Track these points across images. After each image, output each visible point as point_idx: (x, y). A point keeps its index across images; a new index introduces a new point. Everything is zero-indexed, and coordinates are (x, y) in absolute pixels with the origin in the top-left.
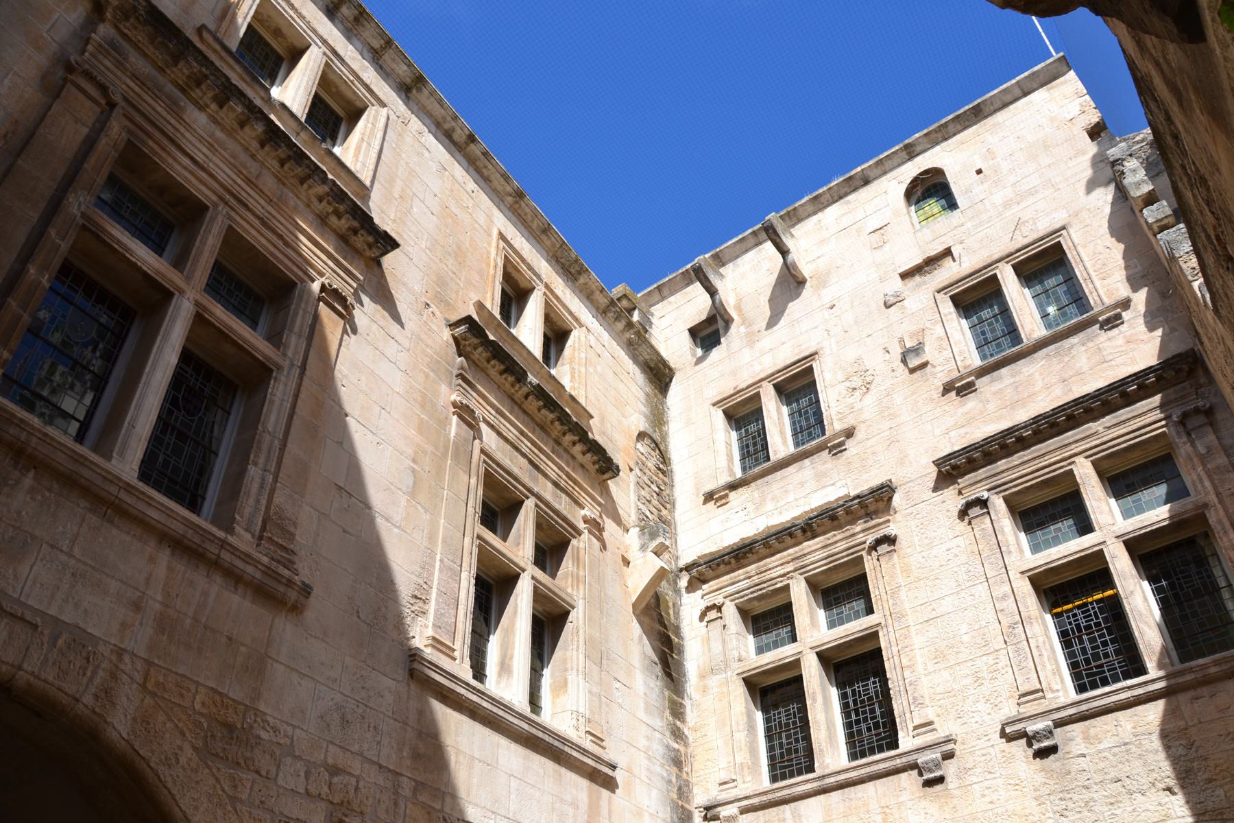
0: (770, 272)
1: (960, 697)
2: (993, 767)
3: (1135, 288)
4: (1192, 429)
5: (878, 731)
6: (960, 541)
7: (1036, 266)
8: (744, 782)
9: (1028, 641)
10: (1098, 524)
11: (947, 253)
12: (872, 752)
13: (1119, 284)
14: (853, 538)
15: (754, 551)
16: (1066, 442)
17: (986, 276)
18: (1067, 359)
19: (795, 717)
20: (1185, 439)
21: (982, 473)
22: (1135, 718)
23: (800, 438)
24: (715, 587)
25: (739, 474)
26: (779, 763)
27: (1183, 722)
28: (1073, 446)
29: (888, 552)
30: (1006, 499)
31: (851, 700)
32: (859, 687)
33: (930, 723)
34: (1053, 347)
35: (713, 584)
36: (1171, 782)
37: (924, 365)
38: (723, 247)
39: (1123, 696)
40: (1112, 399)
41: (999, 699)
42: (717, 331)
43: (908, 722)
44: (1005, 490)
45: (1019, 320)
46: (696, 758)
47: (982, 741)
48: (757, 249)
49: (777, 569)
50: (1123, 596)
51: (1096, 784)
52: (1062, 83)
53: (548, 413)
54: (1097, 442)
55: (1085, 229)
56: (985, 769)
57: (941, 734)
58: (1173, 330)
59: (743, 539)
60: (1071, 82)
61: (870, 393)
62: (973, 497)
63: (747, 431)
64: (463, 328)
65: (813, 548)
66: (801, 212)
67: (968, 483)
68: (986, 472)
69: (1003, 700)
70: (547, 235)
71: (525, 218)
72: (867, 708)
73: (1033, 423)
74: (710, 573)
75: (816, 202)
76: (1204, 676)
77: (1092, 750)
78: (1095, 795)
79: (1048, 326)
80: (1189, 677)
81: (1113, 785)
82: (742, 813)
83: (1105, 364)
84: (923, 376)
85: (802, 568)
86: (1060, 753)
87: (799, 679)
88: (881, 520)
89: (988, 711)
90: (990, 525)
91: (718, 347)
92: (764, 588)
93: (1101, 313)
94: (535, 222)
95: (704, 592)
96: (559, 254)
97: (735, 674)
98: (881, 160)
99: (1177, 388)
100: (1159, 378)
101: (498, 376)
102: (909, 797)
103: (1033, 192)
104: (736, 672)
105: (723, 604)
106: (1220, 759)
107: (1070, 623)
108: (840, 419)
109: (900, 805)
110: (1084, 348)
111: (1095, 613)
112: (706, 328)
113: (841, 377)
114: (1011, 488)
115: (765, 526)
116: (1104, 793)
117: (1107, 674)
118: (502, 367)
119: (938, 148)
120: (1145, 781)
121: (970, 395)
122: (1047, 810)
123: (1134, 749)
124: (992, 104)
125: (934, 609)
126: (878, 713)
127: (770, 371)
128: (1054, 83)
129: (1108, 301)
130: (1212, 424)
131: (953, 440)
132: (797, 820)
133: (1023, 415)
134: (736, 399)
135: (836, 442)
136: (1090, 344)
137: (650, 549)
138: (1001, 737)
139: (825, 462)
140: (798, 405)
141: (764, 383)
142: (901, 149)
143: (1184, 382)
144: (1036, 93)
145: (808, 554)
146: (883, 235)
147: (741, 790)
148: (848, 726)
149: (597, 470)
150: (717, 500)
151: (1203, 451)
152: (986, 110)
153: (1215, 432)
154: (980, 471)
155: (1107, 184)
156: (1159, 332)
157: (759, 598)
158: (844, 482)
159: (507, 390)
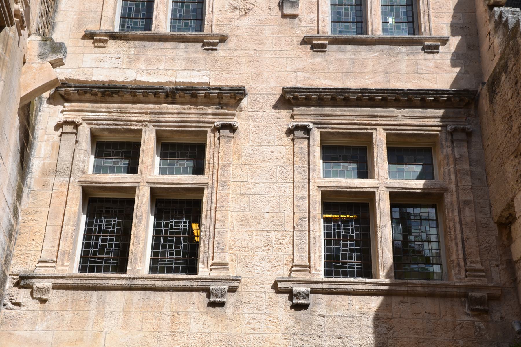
3: (454, 33)
4: (456, 140)
5: (178, 257)
9: (309, 232)
10: (378, 174)
12: (169, 271)
13: (445, 26)
14: (203, 116)
15: (120, 94)
16: (376, 114)
18: (393, 59)
19: (114, 228)
20: (449, 144)
21: (312, 110)
22: (363, 303)
23: (177, 23)
24: (77, 109)
25: (117, 29)
26: (91, 258)
27: (391, 314)
28: (378, 119)
29: (228, 136)
30: (322, 134)
31: (163, 229)
32: (172, 222)
33: (226, 264)
35: (76, 106)
37: (294, 16)
39: (361, 287)
40: (415, 100)
41: (278, 263)
45: (371, 18)
46: (22, 235)
47: (259, 287)
49: (136, 115)
50: (378, 226)
51: (326, 336)
54: (395, 123)
56: (256, 306)
57: (231, 273)
58: (466, 72)
59: (111, 81)
61: (247, 17)
62: (302, 124)
65: (170, 111)
67: (300, 112)
68: (315, 110)
69: (281, 265)
72: (108, 237)
73: (360, 93)
74: (76, 96)
76: (413, 291)
77: (330, 314)
79: (385, 30)
80: (404, 289)
81: (336, 340)
82: (53, 288)
83: (416, 75)
84: (290, 24)
85: (157, 122)
87: (132, 202)
88: (230, 112)
90: (307, 147)
92: (120, 125)
93: (428, 40)
95: (65, 109)
100: (449, 99)
102: (195, 310)
104: (78, 180)
105: (81, 124)
106: (405, 342)
107: (334, 230)
108: (218, 25)
109: (186, 313)
110: (407, 58)
111: (352, 229)
115: (133, 79)
116: (330, 343)
117: (356, 270)
121: (320, 53)
122: (289, 344)
123: (356, 321)
126: (181, 245)
129: (434, 34)
130: (468, 142)
131: (299, 79)
132: (101, 304)
135: (211, 41)
136: (412, 57)
137: (50, 60)
138: (272, 288)
139: (196, 52)
145: (165, 113)
147: (58, 270)
148: (155, 247)
150: (96, 41)
151: (457, 156)
153: (468, 148)
156: (457, 70)
157: (110, 131)
158: (208, 73)
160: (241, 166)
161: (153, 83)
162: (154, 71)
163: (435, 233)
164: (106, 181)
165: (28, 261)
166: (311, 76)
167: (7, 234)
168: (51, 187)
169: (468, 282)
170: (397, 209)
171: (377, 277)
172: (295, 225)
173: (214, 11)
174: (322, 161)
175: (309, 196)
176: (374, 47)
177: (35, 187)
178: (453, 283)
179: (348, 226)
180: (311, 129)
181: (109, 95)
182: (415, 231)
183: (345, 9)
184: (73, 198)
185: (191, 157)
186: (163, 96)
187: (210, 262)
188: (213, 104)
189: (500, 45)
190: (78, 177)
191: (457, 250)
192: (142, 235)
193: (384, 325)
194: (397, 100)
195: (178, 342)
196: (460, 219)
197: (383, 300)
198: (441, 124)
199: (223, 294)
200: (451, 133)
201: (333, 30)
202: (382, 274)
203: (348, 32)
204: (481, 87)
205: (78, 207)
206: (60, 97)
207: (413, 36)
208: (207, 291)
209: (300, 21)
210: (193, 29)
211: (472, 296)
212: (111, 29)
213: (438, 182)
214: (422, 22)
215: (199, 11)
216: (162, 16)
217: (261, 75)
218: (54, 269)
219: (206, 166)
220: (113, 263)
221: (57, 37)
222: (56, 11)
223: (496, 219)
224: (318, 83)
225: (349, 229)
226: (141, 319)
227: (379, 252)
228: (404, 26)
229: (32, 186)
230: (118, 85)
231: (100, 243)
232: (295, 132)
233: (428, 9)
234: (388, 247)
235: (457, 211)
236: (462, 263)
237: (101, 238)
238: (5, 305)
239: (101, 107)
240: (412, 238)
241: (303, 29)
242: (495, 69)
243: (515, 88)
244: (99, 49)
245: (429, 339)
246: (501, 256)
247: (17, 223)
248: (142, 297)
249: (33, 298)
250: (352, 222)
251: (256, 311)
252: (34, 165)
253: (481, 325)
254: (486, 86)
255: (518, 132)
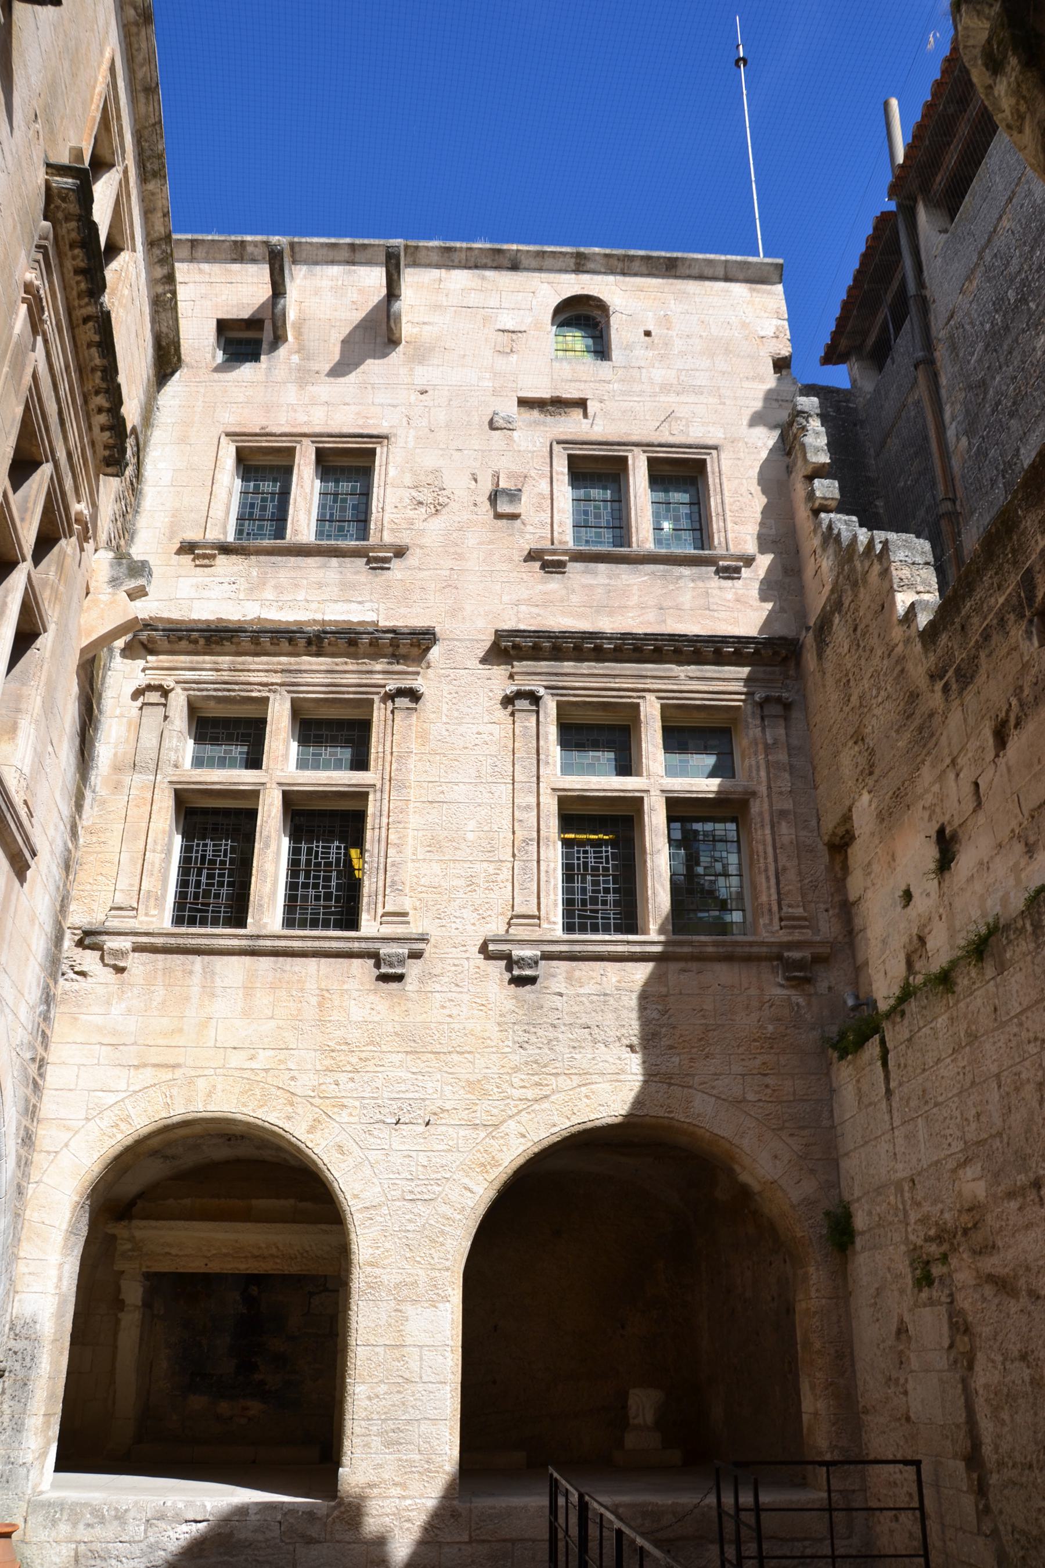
0: (354, 307)
1: (446, 897)
2: (463, 981)
3: (762, 550)
4: (767, 716)
5: (327, 903)
6: (495, 729)
7: (667, 471)
8: (147, 915)
9: (538, 862)
10: (648, 770)
11: (581, 404)
12: (314, 924)
13: (749, 537)
15: (235, 640)
16: (644, 673)
17: (616, 454)
18: (671, 587)
19: (225, 856)
20: (758, 722)
21: (544, 666)
22: (623, 973)
23: (327, 527)
24: (166, 665)
25: (231, 538)
28: (649, 681)
30: (559, 705)
31: (303, 858)
32: (317, 847)
33: (405, 914)
34: (661, 567)
35: (164, 660)
36: (635, 1041)
37: (514, 517)
38: (303, 240)
39: (620, 948)
41: (489, 913)
42: (258, 342)
43: (380, 905)
44: (562, 695)
46: (85, 867)
47: (458, 950)
48: (347, 267)
49: (260, 674)
51: (565, 1025)
52: (764, 292)
53: (97, 355)
54: (675, 687)
55: (736, 462)
57: (414, 929)
58: (782, 610)
59: (220, 620)
60: (774, 297)
61: (439, 517)
62: (527, 688)
63: (257, 487)
64: (68, 182)
65: (314, 667)
66: (422, 256)
67: (524, 670)
68: (548, 667)
70: (147, 99)
71: (135, 53)
73: (620, 639)
74: (166, 645)
75: (446, 255)
78: (560, 1036)
79: (658, 541)
80: (686, 949)
82: (134, 950)
86: (537, 986)
87: (253, 814)
88: (410, 669)
89: (472, 921)
90: (534, 725)
91: (253, 364)
92: (234, 690)
93: (723, 558)
94: (144, 69)
95: (149, 665)
96: (146, 133)
97: (166, 780)
98: (544, 252)
99: (769, 669)
100: (757, 651)
101: (72, 274)
102: (357, 987)
103: (697, 390)
104: (169, 779)
105: (173, 689)
107: (578, 859)
108: (392, 530)
109: (343, 992)
110: (692, 585)
111: (607, 857)
112: (241, 330)
113: (408, 480)
114: (569, 695)
116: (570, 1036)
118: (82, 265)
119: (611, 278)
120: (613, 1033)
122: (507, 1038)
123: (612, 1001)
124: (690, 266)
125: (443, 792)
126: (333, 883)
127: (318, 430)
128: (759, 286)
129: (733, 550)
130: (786, 719)
131: (521, 616)
133: (608, 624)
134: (261, 441)
136: (700, 584)
137: (126, 588)
139: (357, 573)
140: (337, 486)
141: (306, 441)
142: (572, 254)
143: (775, 666)
144: (738, 284)
145: (305, 671)
146: (513, 341)
147: (141, 923)
148: (292, 886)
149: (104, 457)
150: (198, 557)
151: (770, 741)
152: (682, 270)
153: (786, 728)
154: (543, 663)
155: (773, 427)
156: (769, 606)
157: (219, 700)
159: (71, 298)
160: (429, 757)
161: (288, 622)
162: (289, 603)
163: (736, 862)
164: (212, 780)
165: (95, 908)
166: (542, 612)
167: (62, 865)
168: (126, 791)
169: (784, 936)
170: (678, 825)
171: (645, 932)
172: (516, 852)
173: (387, 508)
174: (559, 748)
175: (538, 804)
176: (641, 567)
177: (102, 791)
178: (761, 939)
179: (601, 852)
180: (541, 697)
181: (217, 643)
182: (705, 860)
183: (595, 507)
184: (160, 808)
185: (348, 742)
186: (302, 643)
187: (380, 911)
188: (384, 656)
189: (831, 570)
190: (168, 775)
191: (769, 888)
192: (269, 867)
193: (654, 1006)
194: (677, 651)
195: (331, 1036)
196: (774, 840)
197: (655, 968)
198: (745, 690)
199: (401, 962)
200: (761, 705)
201: (577, 539)
202: (653, 927)
203: (600, 542)
204: (804, 633)
205: (168, 822)
206: (140, 646)
207: (701, 552)
208: (376, 957)
209: (523, 523)
210: (352, 535)
211: (789, 958)
212: (221, 537)
213: (741, 782)
214: (715, 530)
215: (362, 507)
216: (302, 516)
217: (462, 609)
218: (134, 920)
219: (373, 757)
220: (225, 912)
221: (138, 551)
222: (137, 512)
223: (826, 838)
224: (552, 623)
225: (601, 858)
226: (271, 1000)
227: (650, 892)
228: (687, 536)
229: (97, 789)
230: (231, 626)
231: (203, 879)
232: (517, 702)
233: (723, 511)
234: (663, 886)
235: (769, 827)
236: (775, 908)
237: (205, 872)
238: (63, 974)
239: (204, 662)
240: (700, 870)
241: (528, 536)
242: (824, 607)
243: (853, 637)
244: (202, 569)
245: (723, 1025)
246: (832, 895)
247: (76, 847)
248: (272, 965)
249: (105, 965)
250: (607, 847)
251: (455, 989)
252: (101, 755)
253: (800, 1000)
254: (811, 631)
255: (858, 705)
